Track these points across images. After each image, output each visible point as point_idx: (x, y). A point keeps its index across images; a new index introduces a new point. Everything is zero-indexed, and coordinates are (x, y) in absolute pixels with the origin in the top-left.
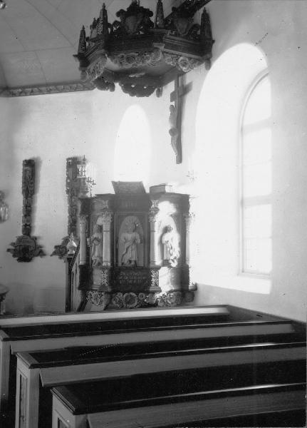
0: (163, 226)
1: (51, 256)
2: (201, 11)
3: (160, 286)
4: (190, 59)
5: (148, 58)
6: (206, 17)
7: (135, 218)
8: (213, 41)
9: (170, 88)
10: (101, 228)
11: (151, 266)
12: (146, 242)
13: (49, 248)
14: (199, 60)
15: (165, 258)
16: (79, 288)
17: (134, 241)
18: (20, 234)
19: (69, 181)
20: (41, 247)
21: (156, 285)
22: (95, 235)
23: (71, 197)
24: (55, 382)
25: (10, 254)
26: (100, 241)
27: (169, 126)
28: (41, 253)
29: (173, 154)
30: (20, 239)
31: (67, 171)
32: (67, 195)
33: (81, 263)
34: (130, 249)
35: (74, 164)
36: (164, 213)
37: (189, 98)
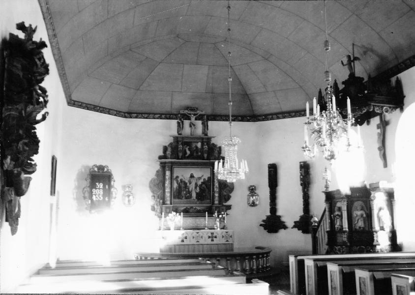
0: (379, 206)
1: (292, 228)
2: (395, 77)
3: (379, 242)
4: (390, 107)
5: (364, 110)
6: (399, 82)
7: (360, 202)
8: (405, 97)
9: (376, 121)
10: (340, 209)
11: (373, 230)
12: (369, 217)
14: (394, 108)
15: (381, 225)
17: (362, 215)
18: (269, 214)
19: (302, 177)
20: (284, 222)
21: (377, 241)
22: (337, 213)
25: (262, 228)
26: (341, 216)
27: (376, 145)
28: (285, 227)
29: (381, 162)
30: (268, 217)
31: (301, 170)
32: (301, 187)
33: (328, 230)
34: (360, 220)
35: (305, 168)
36: (379, 201)
37: (388, 128)
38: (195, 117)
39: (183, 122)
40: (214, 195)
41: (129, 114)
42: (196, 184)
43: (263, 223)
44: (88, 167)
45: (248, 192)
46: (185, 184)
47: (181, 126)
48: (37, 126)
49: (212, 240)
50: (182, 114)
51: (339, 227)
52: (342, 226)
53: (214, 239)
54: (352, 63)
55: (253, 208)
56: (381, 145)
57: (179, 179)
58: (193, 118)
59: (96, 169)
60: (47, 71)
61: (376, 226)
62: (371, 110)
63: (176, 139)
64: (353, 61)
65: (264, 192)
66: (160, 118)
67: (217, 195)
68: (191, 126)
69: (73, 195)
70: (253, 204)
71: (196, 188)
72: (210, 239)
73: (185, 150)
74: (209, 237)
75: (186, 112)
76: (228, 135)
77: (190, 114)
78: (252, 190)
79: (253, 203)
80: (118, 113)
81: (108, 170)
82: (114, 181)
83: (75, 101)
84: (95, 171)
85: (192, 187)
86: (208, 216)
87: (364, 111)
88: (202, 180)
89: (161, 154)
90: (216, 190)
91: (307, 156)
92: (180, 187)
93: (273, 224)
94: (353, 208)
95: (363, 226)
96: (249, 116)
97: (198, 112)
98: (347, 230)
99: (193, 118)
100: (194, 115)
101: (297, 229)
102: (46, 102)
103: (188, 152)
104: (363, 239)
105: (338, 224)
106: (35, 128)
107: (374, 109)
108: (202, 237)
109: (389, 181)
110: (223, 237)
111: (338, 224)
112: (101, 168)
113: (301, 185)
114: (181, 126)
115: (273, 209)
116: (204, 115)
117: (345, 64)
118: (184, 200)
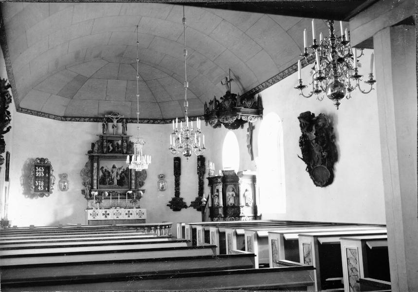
6: (260, 99)
10: (218, 191)
13: (188, 204)
16: (209, 217)
18: (174, 196)
23: (200, 176)
24: (223, 266)
25: (169, 207)
27: (246, 143)
28: (186, 207)
30: (173, 199)
33: (210, 206)
35: (201, 160)
36: (244, 184)
37: (254, 131)
38: (116, 120)
39: (107, 124)
40: (131, 183)
41: (65, 118)
42: (117, 173)
43: (169, 204)
44: (32, 159)
45: (158, 180)
46: (109, 173)
47: (106, 127)
48: (4, 135)
49: (129, 216)
50: (106, 118)
51: (217, 204)
52: (219, 203)
53: (130, 216)
54: (229, 84)
55: (163, 192)
56: (249, 143)
57: (104, 169)
58: (115, 121)
59: (39, 161)
60: (11, 101)
61: (242, 202)
62: (239, 119)
63: (102, 137)
64: (229, 82)
65: (171, 179)
66: (89, 121)
67: (133, 181)
68: (113, 128)
69: (21, 181)
70: (162, 189)
71: (117, 176)
72: (127, 216)
73: (109, 146)
74: (126, 214)
75: (110, 116)
76: (138, 133)
77: (113, 118)
78: (162, 177)
79: (162, 188)
80: (56, 117)
81: (48, 162)
82: (53, 171)
83: (22, 108)
84: (38, 163)
85: (114, 175)
86: (128, 198)
87: (234, 120)
88: (122, 170)
89: (90, 149)
90: (133, 178)
91: (204, 153)
92: (104, 175)
93: (177, 204)
94: (227, 190)
95: (233, 203)
96: (160, 120)
97: (119, 116)
98: (222, 205)
99: (115, 121)
100: (116, 118)
101: (193, 208)
102: (10, 120)
103: (111, 148)
104: (233, 211)
105: (216, 201)
106: (3, 137)
107: (241, 117)
108: (121, 214)
109: (252, 170)
110: (137, 214)
111: (216, 201)
112: (42, 160)
113: (198, 173)
114: (106, 127)
115: (177, 193)
116: (123, 119)
117: (223, 83)
118: (108, 186)
